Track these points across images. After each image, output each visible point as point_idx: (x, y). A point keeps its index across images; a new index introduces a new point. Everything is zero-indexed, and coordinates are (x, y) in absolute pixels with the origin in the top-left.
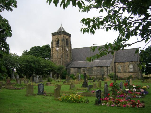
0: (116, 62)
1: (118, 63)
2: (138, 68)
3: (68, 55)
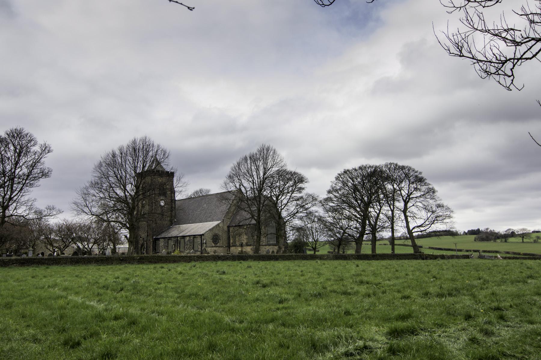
1: (233, 228)
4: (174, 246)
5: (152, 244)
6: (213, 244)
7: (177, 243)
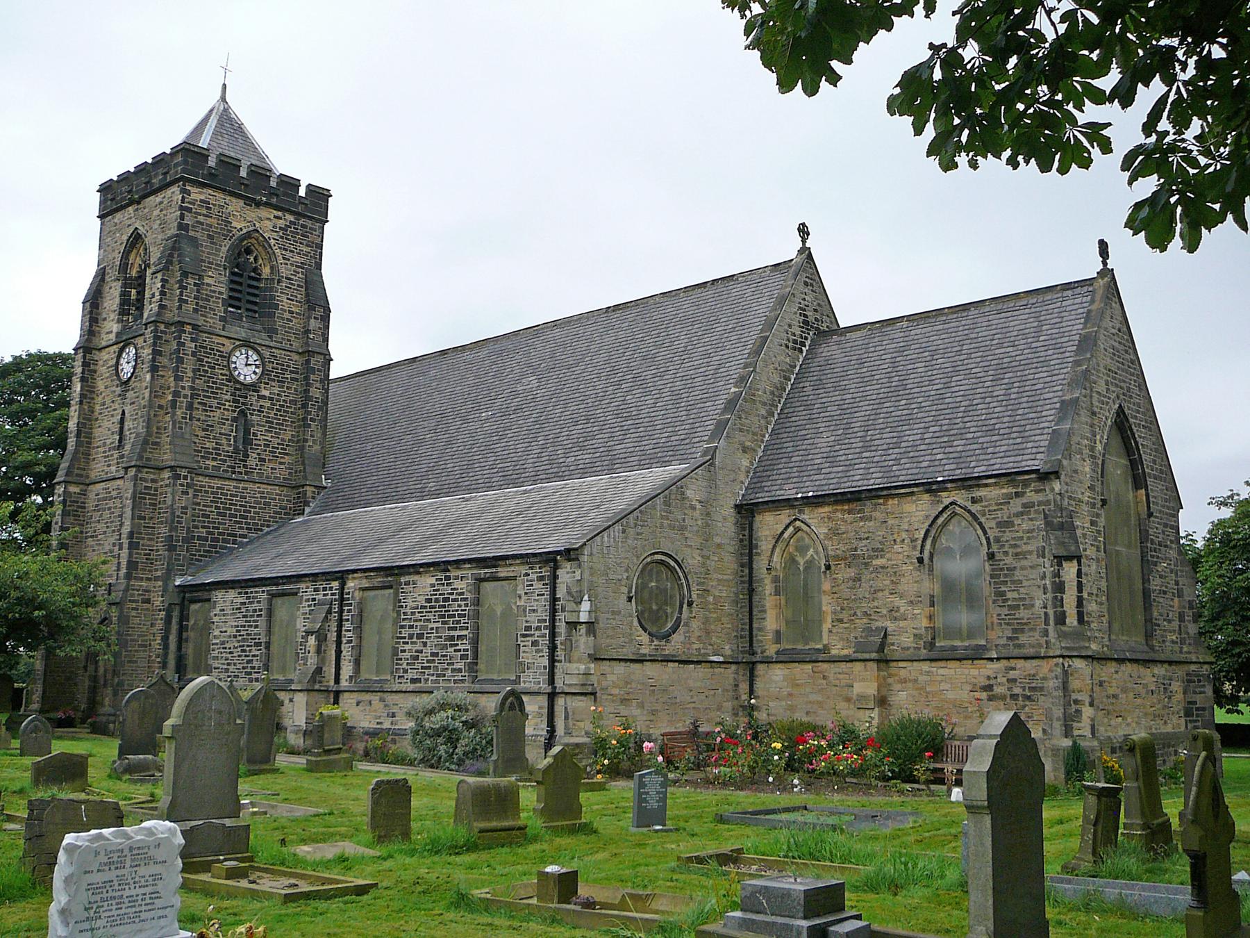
0: (763, 497)
1: (784, 516)
2: (1060, 587)
3: (261, 434)
4: (312, 640)
5: (160, 624)
6: (645, 638)
7: (340, 622)
